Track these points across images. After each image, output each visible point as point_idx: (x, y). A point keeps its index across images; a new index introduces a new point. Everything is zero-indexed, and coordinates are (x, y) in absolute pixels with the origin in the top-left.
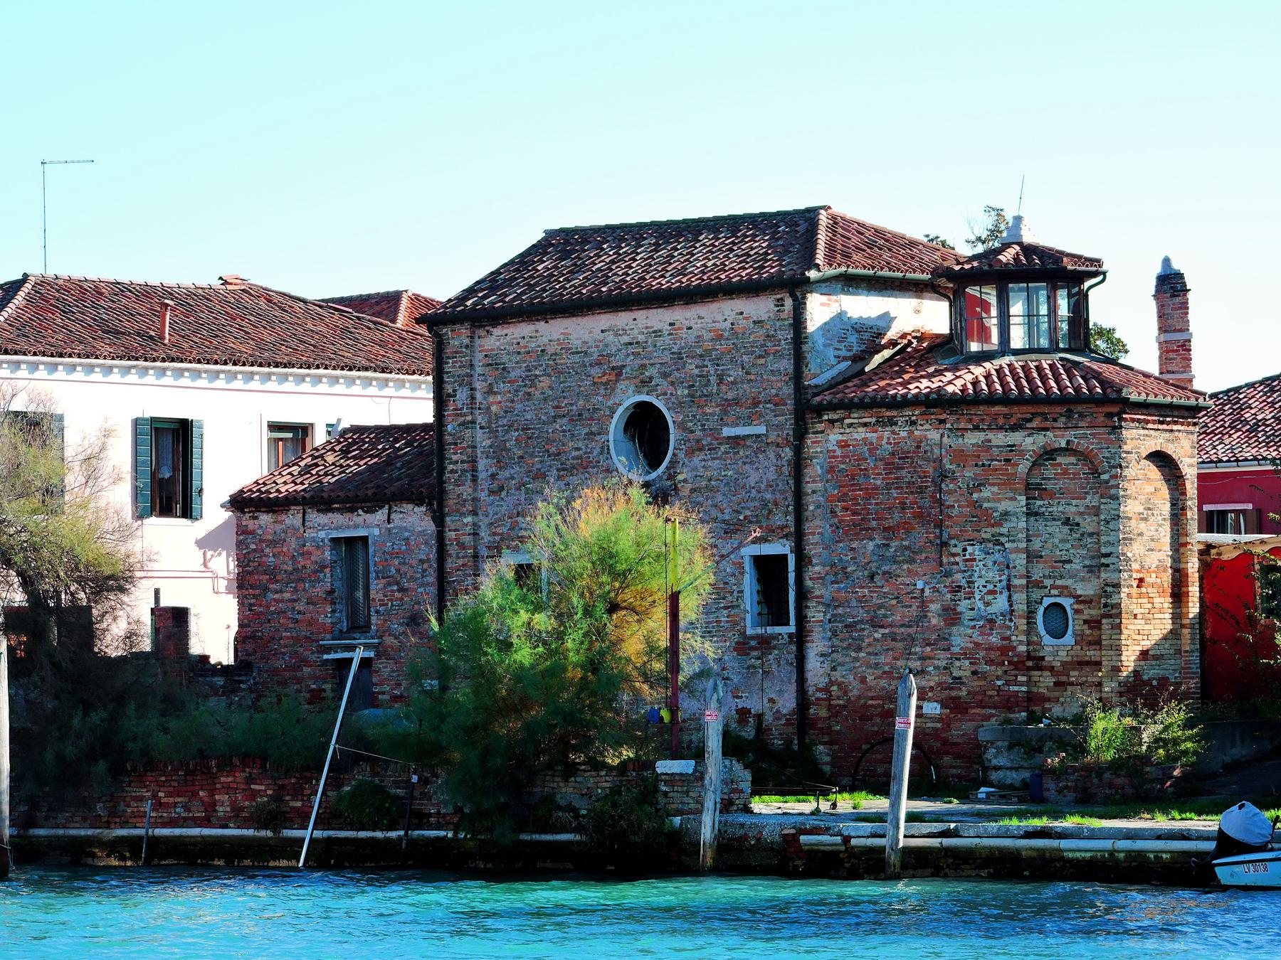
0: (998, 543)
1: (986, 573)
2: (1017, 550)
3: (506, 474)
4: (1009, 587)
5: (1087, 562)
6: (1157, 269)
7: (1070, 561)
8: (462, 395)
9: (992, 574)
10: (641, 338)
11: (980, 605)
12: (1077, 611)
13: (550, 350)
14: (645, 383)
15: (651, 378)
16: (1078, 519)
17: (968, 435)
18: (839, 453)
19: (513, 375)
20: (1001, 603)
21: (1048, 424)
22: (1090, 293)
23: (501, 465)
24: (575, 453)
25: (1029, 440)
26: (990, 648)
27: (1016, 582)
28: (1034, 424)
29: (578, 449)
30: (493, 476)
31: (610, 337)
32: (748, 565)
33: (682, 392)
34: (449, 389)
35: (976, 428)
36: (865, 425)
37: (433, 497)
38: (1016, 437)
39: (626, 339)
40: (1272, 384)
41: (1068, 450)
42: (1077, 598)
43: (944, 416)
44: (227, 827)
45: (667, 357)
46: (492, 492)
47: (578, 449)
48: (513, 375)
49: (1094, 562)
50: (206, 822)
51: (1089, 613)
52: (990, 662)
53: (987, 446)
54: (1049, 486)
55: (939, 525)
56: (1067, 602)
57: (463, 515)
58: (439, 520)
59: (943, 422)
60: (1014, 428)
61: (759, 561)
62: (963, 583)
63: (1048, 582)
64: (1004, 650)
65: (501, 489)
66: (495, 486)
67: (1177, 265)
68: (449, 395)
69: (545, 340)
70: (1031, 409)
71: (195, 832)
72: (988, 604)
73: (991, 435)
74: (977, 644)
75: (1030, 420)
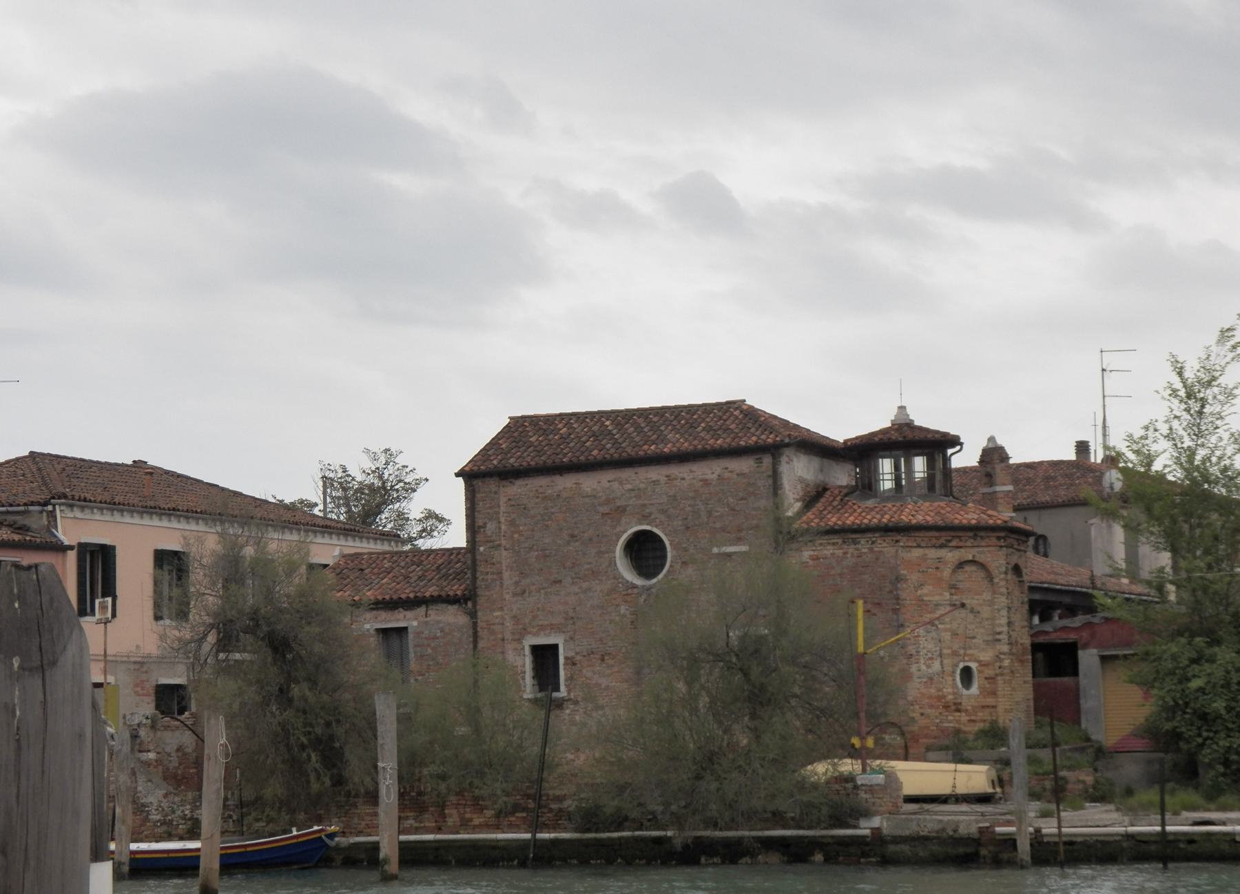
0: (933, 625)
1: (927, 644)
2: (946, 630)
3: (528, 581)
4: (941, 655)
5: (986, 638)
6: (984, 444)
7: (974, 638)
8: (491, 527)
9: (931, 646)
10: (642, 486)
11: (923, 667)
12: (980, 672)
13: (564, 495)
14: (645, 518)
15: (650, 514)
16: (979, 609)
17: (914, 550)
18: (811, 563)
19: (532, 512)
20: (936, 666)
21: (961, 544)
22: (953, 458)
23: (523, 575)
24: (587, 566)
25: (950, 554)
26: (930, 697)
27: (946, 651)
28: (954, 543)
29: (590, 563)
30: (516, 583)
31: (616, 485)
32: (527, 651)
33: (678, 523)
34: (480, 522)
35: (919, 546)
36: (834, 544)
37: (466, 600)
38: (943, 553)
39: (629, 486)
40: (1177, 507)
41: (973, 562)
42: (979, 662)
43: (899, 537)
44: (458, 833)
45: (664, 499)
46: (515, 595)
47: (590, 563)
48: (532, 512)
49: (990, 638)
50: (439, 830)
51: (989, 672)
52: (931, 706)
53: (924, 558)
54: (960, 585)
55: (896, 611)
56: (973, 665)
57: (494, 610)
58: (473, 615)
59: (897, 541)
60: (942, 546)
61: (536, 649)
62: (914, 652)
63: (962, 652)
64: (939, 698)
65: (524, 592)
66: (518, 590)
67: (1000, 441)
68: (480, 527)
69: (560, 488)
70: (953, 534)
71: (430, 837)
72: (929, 667)
73: (927, 551)
74: (923, 694)
75: (950, 541)
